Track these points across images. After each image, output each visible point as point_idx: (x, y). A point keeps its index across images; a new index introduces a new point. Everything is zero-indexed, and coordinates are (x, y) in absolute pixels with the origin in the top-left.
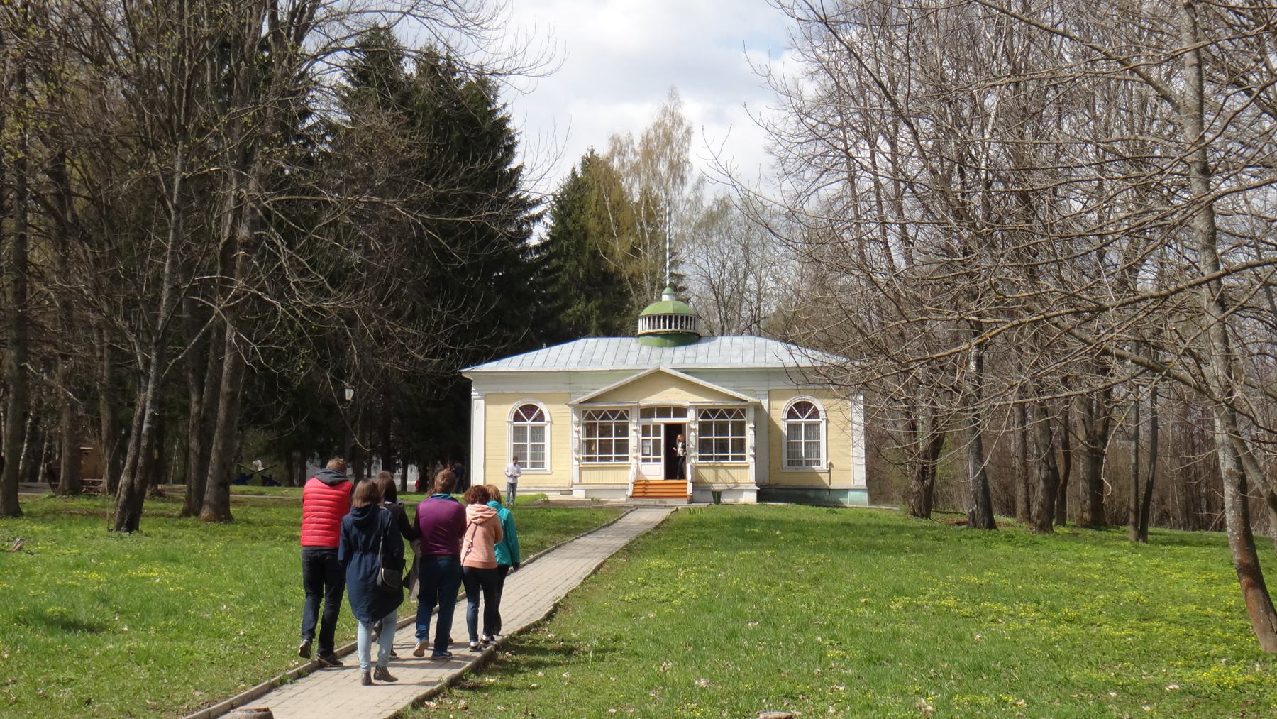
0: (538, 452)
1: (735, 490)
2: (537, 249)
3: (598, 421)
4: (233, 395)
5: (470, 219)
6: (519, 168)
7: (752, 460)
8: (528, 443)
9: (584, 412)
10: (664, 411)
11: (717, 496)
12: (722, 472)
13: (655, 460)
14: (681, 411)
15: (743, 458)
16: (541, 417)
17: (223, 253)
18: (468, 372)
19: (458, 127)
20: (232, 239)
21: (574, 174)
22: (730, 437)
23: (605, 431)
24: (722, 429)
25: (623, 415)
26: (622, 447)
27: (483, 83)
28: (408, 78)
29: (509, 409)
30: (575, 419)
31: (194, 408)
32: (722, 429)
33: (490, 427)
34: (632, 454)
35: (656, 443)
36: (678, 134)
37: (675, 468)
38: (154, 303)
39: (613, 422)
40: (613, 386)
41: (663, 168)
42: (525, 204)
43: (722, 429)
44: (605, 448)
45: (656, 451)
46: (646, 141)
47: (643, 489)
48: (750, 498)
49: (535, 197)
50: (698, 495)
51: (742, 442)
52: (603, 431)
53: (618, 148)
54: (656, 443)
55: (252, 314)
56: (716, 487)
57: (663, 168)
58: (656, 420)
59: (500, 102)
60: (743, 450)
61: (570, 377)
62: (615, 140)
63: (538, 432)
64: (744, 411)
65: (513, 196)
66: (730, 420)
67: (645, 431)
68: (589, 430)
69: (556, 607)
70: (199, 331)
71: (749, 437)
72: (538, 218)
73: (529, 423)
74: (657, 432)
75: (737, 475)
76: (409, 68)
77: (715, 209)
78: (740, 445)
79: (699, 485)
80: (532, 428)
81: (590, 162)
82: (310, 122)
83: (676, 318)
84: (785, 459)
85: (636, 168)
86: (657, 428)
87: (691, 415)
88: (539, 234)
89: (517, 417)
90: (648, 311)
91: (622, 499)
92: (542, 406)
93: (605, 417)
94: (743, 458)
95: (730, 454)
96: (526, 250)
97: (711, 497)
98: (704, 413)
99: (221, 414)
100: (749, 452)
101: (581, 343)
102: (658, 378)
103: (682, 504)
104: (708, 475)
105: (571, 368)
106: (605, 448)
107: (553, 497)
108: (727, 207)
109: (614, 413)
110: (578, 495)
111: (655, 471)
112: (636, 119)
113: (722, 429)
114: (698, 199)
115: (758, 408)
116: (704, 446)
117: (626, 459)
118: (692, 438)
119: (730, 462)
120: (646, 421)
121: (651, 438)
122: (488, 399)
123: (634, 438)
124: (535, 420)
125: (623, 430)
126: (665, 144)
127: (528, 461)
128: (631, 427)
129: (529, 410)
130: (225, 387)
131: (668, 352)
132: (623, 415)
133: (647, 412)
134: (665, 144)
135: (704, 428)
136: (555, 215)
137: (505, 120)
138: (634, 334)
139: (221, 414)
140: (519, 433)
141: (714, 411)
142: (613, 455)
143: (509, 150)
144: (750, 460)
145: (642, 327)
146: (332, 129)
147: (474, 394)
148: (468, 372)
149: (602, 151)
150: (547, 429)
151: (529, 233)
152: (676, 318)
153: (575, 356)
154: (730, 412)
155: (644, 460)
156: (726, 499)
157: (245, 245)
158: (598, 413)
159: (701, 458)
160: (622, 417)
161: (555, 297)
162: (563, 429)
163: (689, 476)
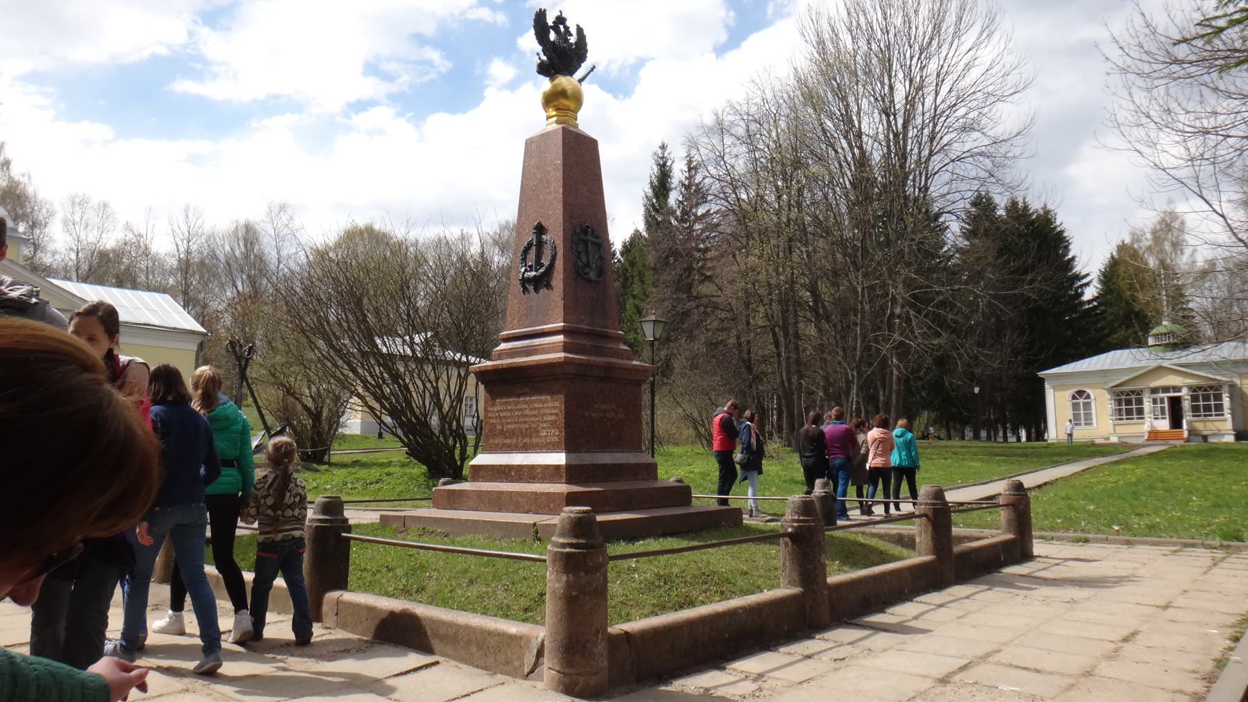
0: (1088, 418)
1: (1219, 434)
2: (1089, 302)
4: (899, 391)
5: (1016, 292)
6: (1073, 258)
11: (1205, 438)
12: (1209, 424)
14: (1177, 389)
16: (1088, 397)
17: (889, 321)
18: (1042, 374)
19: (1030, 242)
20: (892, 314)
21: (1112, 257)
23: (1129, 402)
24: (1206, 398)
25: (1139, 393)
26: (1140, 412)
27: (1047, 212)
28: (1001, 216)
29: (1069, 393)
30: (1108, 396)
31: (882, 398)
32: (1206, 398)
33: (1057, 404)
34: (1146, 415)
35: (1163, 409)
36: (1176, 224)
37: (1176, 422)
38: (855, 349)
39: (1133, 397)
40: (1132, 376)
41: (1168, 247)
42: (1078, 277)
43: (1206, 398)
44: (1129, 412)
45: (1163, 412)
46: (1154, 232)
47: (1154, 435)
48: (1230, 439)
49: (1083, 273)
50: (1192, 438)
52: (1128, 402)
53: (1136, 238)
54: (1163, 409)
55: (902, 350)
56: (1205, 433)
57: (1168, 247)
58: (1161, 395)
59: (1058, 223)
60: (1222, 410)
61: (1105, 373)
62: (1133, 234)
63: (1087, 406)
67: (1155, 401)
68: (1119, 402)
69: (1045, 484)
71: (1226, 401)
72: (1087, 284)
73: (1081, 401)
74: (1162, 401)
75: (1220, 425)
77: (706, 289)
78: (1219, 408)
79: (1192, 432)
81: (1122, 248)
82: (945, 249)
85: (1149, 248)
86: (1162, 401)
88: (1089, 293)
89: (1074, 397)
90: (1154, 331)
91: (1140, 441)
92: (1088, 391)
96: (1083, 303)
97: (1201, 439)
98: (1190, 388)
99: (894, 400)
101: (1112, 353)
102: (1160, 370)
103: (1181, 442)
104: (1199, 426)
105: (1106, 367)
106: (1129, 412)
107: (1098, 441)
108: (1214, 265)
109: (1133, 392)
110: (1114, 439)
111: (1164, 425)
112: (1146, 220)
113: (1206, 398)
114: (1194, 262)
115: (1232, 386)
116: (1195, 409)
118: (1186, 405)
120: (1154, 396)
122: (1055, 388)
123: (1147, 405)
125: (1140, 402)
126: (1169, 229)
128: (1145, 400)
129: (1081, 393)
130: (895, 387)
131: (1169, 354)
132: (1139, 393)
133: (1154, 390)
134: (1169, 229)
135: (1194, 398)
136: (1101, 281)
137: (1062, 232)
139: (894, 400)
140: (1075, 407)
141: (1200, 388)
143: (1067, 248)
144: (1228, 417)
145: (1151, 341)
146: (959, 250)
147: (1047, 386)
148: (1042, 374)
149: (1128, 241)
150: (1093, 404)
151: (1082, 294)
153: (1108, 361)
154: (1211, 387)
156: (1211, 440)
157: (899, 317)
158: (1122, 393)
160: (1138, 394)
161: (1103, 328)
162: (1102, 403)
163: (1185, 426)
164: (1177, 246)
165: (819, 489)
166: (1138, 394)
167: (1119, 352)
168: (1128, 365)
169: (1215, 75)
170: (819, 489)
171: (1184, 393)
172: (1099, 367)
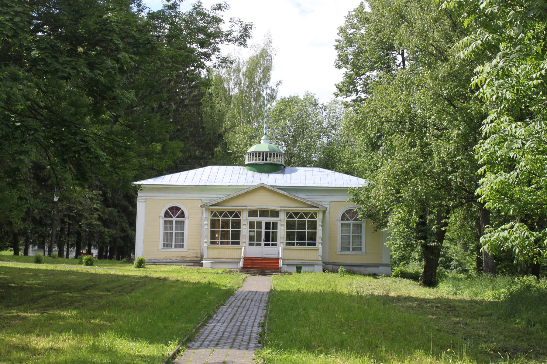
3: (220, 218)
7: (320, 246)
8: (174, 232)
9: (212, 212)
10: (264, 213)
13: (257, 244)
14: (275, 214)
16: (182, 215)
22: (231, 229)
26: (236, 236)
64: (316, 214)
65: (368, 354)
67: (251, 225)
70: (485, 263)
73: (174, 219)
78: (313, 237)
80: (176, 221)
84: (339, 246)
86: (259, 224)
89: (167, 214)
93: (301, 217)
94: (315, 244)
95: (306, 242)
100: (319, 240)
101: (208, 168)
106: (224, 235)
109: (231, 213)
119: (306, 247)
121: (255, 230)
123: (245, 231)
124: (178, 217)
125: (237, 224)
127: (173, 243)
133: (253, 213)
135: (290, 225)
138: (242, 164)
140: (168, 224)
141: (296, 214)
142: (230, 241)
153: (205, 177)
154: (306, 214)
155: (250, 244)
158: (221, 213)
164: (266, 78)
165: (351, 72)
166: (312, 217)
167: (215, 168)
168: (226, 182)
169: (90, 143)
170: (351, 72)
171: (282, 221)
172: (188, 183)
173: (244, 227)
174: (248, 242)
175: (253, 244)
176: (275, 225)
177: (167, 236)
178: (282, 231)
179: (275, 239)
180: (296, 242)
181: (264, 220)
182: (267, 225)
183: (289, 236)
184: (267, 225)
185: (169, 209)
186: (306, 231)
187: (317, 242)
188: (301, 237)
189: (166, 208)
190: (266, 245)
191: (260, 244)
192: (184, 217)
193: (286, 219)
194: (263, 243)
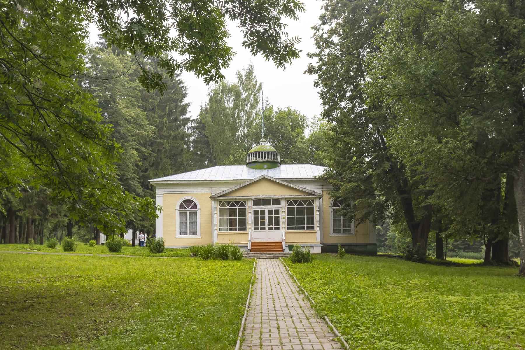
3: (296, 206)
7: (318, 229)
8: (188, 221)
10: (266, 201)
13: (262, 229)
14: (277, 202)
15: (313, 228)
16: (195, 206)
22: (296, 216)
25: (242, 203)
51: (313, 219)
60: (313, 223)
61: (210, 184)
66: (237, 207)
67: (256, 212)
76: (327, 107)
78: (311, 221)
83: (262, 153)
86: (263, 212)
87: (283, 203)
89: (181, 206)
93: (233, 205)
94: (313, 228)
95: (260, 227)
98: (289, 202)
100: (316, 224)
109: (237, 202)
117: (245, 229)
123: (250, 218)
124: (191, 208)
125: (243, 212)
133: (257, 202)
135: (290, 211)
141: (296, 201)
142: (238, 227)
144: (317, 229)
152: (262, 153)
154: (305, 201)
155: (255, 229)
159: (288, 228)
160: (242, 205)
162: (208, 211)
171: (283, 207)
173: (250, 214)
174: (253, 227)
175: (258, 229)
176: (277, 212)
177: (183, 224)
178: (283, 216)
179: (277, 223)
180: (238, 227)
181: (267, 208)
182: (270, 212)
183: (290, 221)
184: (270, 212)
185: (183, 202)
186: (305, 216)
187: (315, 226)
188: (301, 221)
189: (181, 201)
190: (269, 229)
191: (264, 229)
192: (196, 208)
193: (287, 206)
194: (267, 227)
